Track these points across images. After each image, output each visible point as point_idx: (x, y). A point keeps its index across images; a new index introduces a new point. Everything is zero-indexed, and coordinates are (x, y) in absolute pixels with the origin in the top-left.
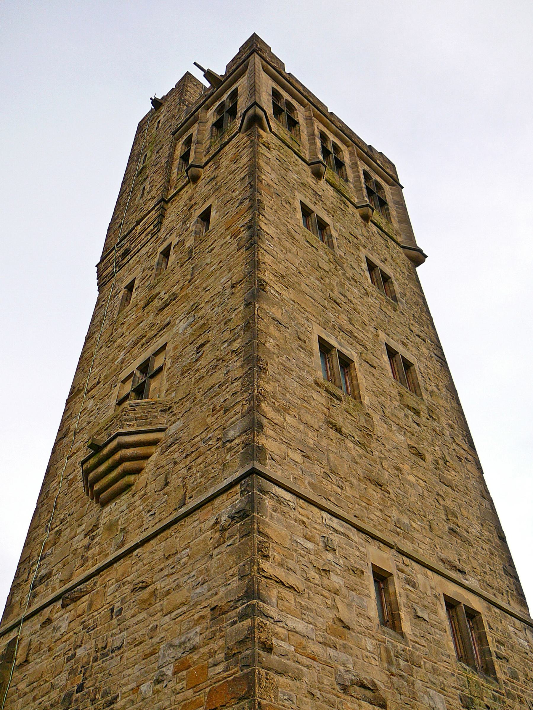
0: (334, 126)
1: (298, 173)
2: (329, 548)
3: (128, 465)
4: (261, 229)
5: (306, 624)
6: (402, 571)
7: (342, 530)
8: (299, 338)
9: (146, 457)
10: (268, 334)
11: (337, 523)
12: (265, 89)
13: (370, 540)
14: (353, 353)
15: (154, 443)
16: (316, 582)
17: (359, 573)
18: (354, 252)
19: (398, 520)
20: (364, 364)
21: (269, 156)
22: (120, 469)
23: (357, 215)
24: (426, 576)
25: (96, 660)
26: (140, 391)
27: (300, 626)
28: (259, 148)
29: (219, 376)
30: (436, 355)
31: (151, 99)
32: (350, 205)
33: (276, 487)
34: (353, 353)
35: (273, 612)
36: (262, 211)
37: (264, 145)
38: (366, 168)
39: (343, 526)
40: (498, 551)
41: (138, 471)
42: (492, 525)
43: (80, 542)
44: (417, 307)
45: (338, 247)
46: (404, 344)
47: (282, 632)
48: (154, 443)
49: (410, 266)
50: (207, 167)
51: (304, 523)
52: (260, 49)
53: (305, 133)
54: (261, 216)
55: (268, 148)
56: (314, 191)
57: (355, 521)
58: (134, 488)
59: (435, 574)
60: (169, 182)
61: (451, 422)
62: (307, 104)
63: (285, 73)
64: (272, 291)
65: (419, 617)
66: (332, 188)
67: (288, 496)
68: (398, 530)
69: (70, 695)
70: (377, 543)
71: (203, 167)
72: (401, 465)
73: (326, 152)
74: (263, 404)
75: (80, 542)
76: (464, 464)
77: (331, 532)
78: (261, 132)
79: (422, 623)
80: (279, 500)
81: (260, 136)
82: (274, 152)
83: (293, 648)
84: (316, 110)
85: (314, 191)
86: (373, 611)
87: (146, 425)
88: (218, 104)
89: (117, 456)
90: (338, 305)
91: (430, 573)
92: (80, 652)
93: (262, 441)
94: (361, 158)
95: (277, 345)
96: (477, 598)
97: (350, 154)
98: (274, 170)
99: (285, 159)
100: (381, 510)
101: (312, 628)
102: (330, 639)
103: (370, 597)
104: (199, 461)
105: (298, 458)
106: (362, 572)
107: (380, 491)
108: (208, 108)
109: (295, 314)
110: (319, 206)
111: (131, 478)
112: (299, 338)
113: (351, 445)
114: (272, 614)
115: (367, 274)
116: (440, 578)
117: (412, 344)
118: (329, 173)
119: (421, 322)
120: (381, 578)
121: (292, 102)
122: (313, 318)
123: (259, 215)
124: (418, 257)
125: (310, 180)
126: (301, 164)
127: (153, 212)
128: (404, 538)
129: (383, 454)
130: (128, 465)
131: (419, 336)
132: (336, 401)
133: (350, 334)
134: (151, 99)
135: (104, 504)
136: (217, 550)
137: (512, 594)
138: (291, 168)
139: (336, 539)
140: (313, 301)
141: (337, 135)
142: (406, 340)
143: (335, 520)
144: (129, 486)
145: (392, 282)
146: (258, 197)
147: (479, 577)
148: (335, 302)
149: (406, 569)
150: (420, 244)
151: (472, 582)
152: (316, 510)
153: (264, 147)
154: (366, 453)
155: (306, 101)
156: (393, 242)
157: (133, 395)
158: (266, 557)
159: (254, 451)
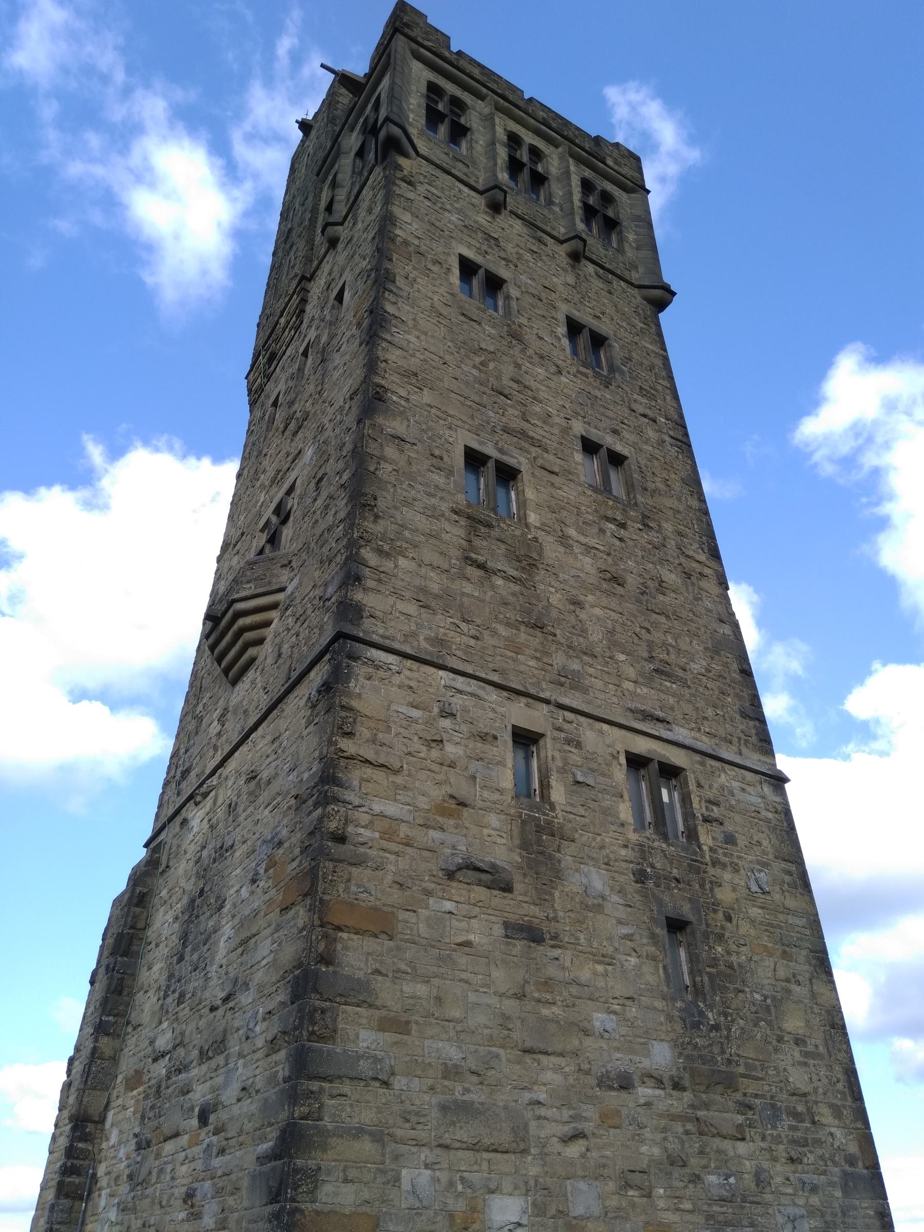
0: (532, 121)
1: (460, 211)
2: (444, 714)
3: (249, 636)
4: (386, 312)
5: (401, 806)
6: (560, 729)
7: (469, 689)
8: (432, 455)
9: (267, 624)
10: (382, 458)
11: (462, 683)
12: (414, 88)
13: (513, 696)
14: (522, 460)
15: (274, 606)
16: (422, 755)
17: (490, 739)
18: (545, 314)
19: (564, 667)
20: (539, 472)
21: (411, 195)
22: (240, 643)
23: (560, 255)
24: (601, 732)
25: (214, 861)
26: (273, 540)
27: (391, 809)
28: (395, 188)
29: (330, 518)
30: (672, 438)
31: (297, 122)
32: (549, 241)
33: (373, 651)
34: (522, 460)
35: (349, 796)
36: (390, 286)
37: (405, 181)
38: (588, 173)
39: (469, 684)
40: (734, 688)
41: (260, 641)
42: (730, 656)
43: (215, 727)
44: (649, 373)
45: (518, 311)
46: (615, 432)
47: (364, 818)
48: (274, 606)
49: (649, 313)
50: (346, 223)
51: (411, 687)
52: (407, 26)
53: (481, 142)
54: (387, 293)
55: (410, 183)
56: (486, 234)
57: (495, 678)
58: (257, 662)
59: (614, 728)
60: (312, 249)
61: (682, 527)
62: (487, 95)
63: (451, 52)
64: (395, 398)
65: (579, 782)
66: (519, 222)
67: (391, 658)
68: (563, 679)
69: (193, 901)
70: (524, 700)
71: (342, 224)
72: (582, 598)
73: (515, 166)
74: (363, 551)
75: (215, 727)
76: (695, 581)
77: (452, 694)
78: (402, 161)
79: (585, 789)
80: (371, 662)
81: (399, 168)
82: (421, 189)
83: (377, 835)
84: (502, 101)
85: (486, 234)
86: (507, 780)
87: (265, 586)
88: (362, 120)
89: (235, 627)
90: (506, 397)
91: (605, 727)
92: (205, 853)
93: (359, 596)
94: (579, 160)
95: (394, 470)
96: (683, 752)
97: (560, 158)
98: (417, 217)
99: (439, 194)
100: (537, 658)
101: (408, 810)
102: (434, 819)
103: (505, 766)
104: (305, 625)
105: (412, 609)
106: (495, 738)
107: (540, 634)
108: (352, 129)
109: (430, 423)
110: (494, 255)
111: (251, 652)
112: (432, 455)
113: (500, 582)
114: (347, 798)
115: (565, 342)
116: (623, 732)
117: (631, 429)
118: (516, 201)
119: (653, 395)
120: (525, 739)
121: (462, 97)
122: (459, 423)
123: (384, 293)
124: (660, 297)
125: (482, 219)
126: (469, 195)
127: (295, 296)
128: (572, 688)
129: (552, 587)
130: (249, 636)
131: (645, 416)
132: (483, 529)
133: (523, 434)
134: (297, 122)
135: (234, 683)
136: (307, 730)
137: (746, 742)
138: (448, 207)
139: (458, 701)
140: (462, 399)
141: (538, 133)
142: (621, 425)
143: (461, 679)
144: (253, 660)
145: (610, 346)
146: (387, 265)
147: (693, 725)
148: (501, 393)
149: (566, 726)
150: (668, 277)
151: (681, 734)
152: (432, 670)
153: (403, 184)
154: (524, 590)
155: (484, 90)
156: (622, 283)
157: (268, 547)
158: (349, 735)
159: (349, 611)
